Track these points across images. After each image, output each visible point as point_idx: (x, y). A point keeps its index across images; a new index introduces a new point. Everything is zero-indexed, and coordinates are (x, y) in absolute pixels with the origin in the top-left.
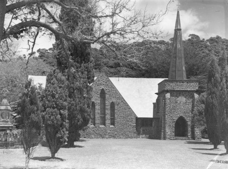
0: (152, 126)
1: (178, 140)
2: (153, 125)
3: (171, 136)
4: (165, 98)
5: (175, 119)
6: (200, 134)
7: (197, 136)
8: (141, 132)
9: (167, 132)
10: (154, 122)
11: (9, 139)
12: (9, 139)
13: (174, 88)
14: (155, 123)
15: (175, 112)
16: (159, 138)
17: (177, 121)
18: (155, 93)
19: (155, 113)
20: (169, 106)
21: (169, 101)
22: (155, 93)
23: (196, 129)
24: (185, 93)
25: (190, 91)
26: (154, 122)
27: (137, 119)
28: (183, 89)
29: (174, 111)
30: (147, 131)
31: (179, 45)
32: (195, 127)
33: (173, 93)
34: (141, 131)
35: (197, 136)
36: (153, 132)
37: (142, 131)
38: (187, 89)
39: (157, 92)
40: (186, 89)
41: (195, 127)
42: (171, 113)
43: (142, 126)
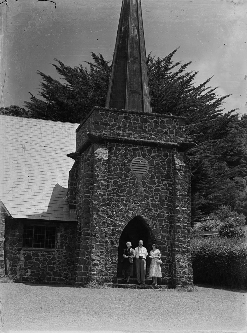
0: (53, 247)
1: (127, 288)
2: (58, 243)
3: (107, 275)
4: (92, 162)
5: (120, 223)
6: (189, 270)
7: (183, 277)
8: (21, 263)
9: (96, 262)
10: (59, 235)
11: (93, 111)
12: (93, 111)
13: (118, 134)
14: (62, 236)
15: (120, 205)
16: (70, 281)
17: (124, 230)
18: (68, 155)
19: (120, 21)
20: (105, 183)
21: (103, 169)
22: (68, 155)
23: (178, 256)
24: (149, 151)
25: (162, 145)
26: (59, 235)
27: (12, 223)
28: (144, 138)
29: (119, 202)
30: (37, 259)
31: (134, 29)
32: (177, 249)
33: (116, 149)
34: (19, 259)
35: (183, 277)
36: (54, 263)
37: (22, 259)
38: (155, 139)
39: (73, 150)
40: (153, 139)
41: (177, 249)
42: (108, 204)
43: (24, 245)
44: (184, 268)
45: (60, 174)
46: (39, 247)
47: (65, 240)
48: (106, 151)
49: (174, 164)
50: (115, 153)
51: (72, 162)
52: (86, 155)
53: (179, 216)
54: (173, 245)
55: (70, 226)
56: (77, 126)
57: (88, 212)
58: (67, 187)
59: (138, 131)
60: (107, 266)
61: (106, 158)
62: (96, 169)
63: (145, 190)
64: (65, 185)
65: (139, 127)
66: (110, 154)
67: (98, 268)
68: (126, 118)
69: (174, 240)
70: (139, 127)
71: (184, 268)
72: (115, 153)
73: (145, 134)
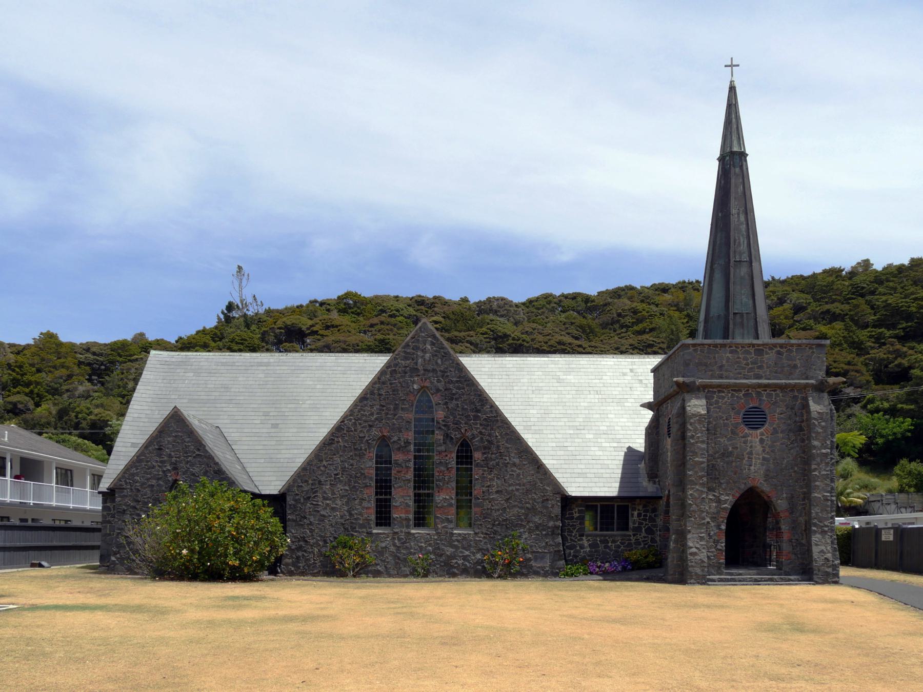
6: (834, 555)
9: (694, 550)
44: (825, 553)
45: (632, 429)
46: (607, 530)
47: (645, 520)
48: (704, 402)
49: (809, 412)
50: (717, 402)
51: (649, 414)
52: (672, 409)
53: (817, 483)
54: (808, 524)
55: (650, 501)
56: (654, 361)
57: (681, 483)
58: (642, 450)
59: (751, 368)
60: (710, 554)
61: (704, 412)
62: (690, 427)
63: (764, 451)
64: (640, 444)
65: (752, 363)
66: (709, 404)
67: (698, 557)
68: (731, 352)
69: (810, 518)
70: (752, 363)
71: (825, 553)
72: (717, 402)
73: (761, 372)
